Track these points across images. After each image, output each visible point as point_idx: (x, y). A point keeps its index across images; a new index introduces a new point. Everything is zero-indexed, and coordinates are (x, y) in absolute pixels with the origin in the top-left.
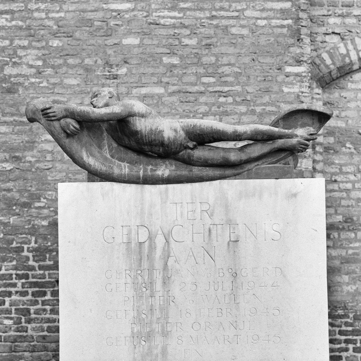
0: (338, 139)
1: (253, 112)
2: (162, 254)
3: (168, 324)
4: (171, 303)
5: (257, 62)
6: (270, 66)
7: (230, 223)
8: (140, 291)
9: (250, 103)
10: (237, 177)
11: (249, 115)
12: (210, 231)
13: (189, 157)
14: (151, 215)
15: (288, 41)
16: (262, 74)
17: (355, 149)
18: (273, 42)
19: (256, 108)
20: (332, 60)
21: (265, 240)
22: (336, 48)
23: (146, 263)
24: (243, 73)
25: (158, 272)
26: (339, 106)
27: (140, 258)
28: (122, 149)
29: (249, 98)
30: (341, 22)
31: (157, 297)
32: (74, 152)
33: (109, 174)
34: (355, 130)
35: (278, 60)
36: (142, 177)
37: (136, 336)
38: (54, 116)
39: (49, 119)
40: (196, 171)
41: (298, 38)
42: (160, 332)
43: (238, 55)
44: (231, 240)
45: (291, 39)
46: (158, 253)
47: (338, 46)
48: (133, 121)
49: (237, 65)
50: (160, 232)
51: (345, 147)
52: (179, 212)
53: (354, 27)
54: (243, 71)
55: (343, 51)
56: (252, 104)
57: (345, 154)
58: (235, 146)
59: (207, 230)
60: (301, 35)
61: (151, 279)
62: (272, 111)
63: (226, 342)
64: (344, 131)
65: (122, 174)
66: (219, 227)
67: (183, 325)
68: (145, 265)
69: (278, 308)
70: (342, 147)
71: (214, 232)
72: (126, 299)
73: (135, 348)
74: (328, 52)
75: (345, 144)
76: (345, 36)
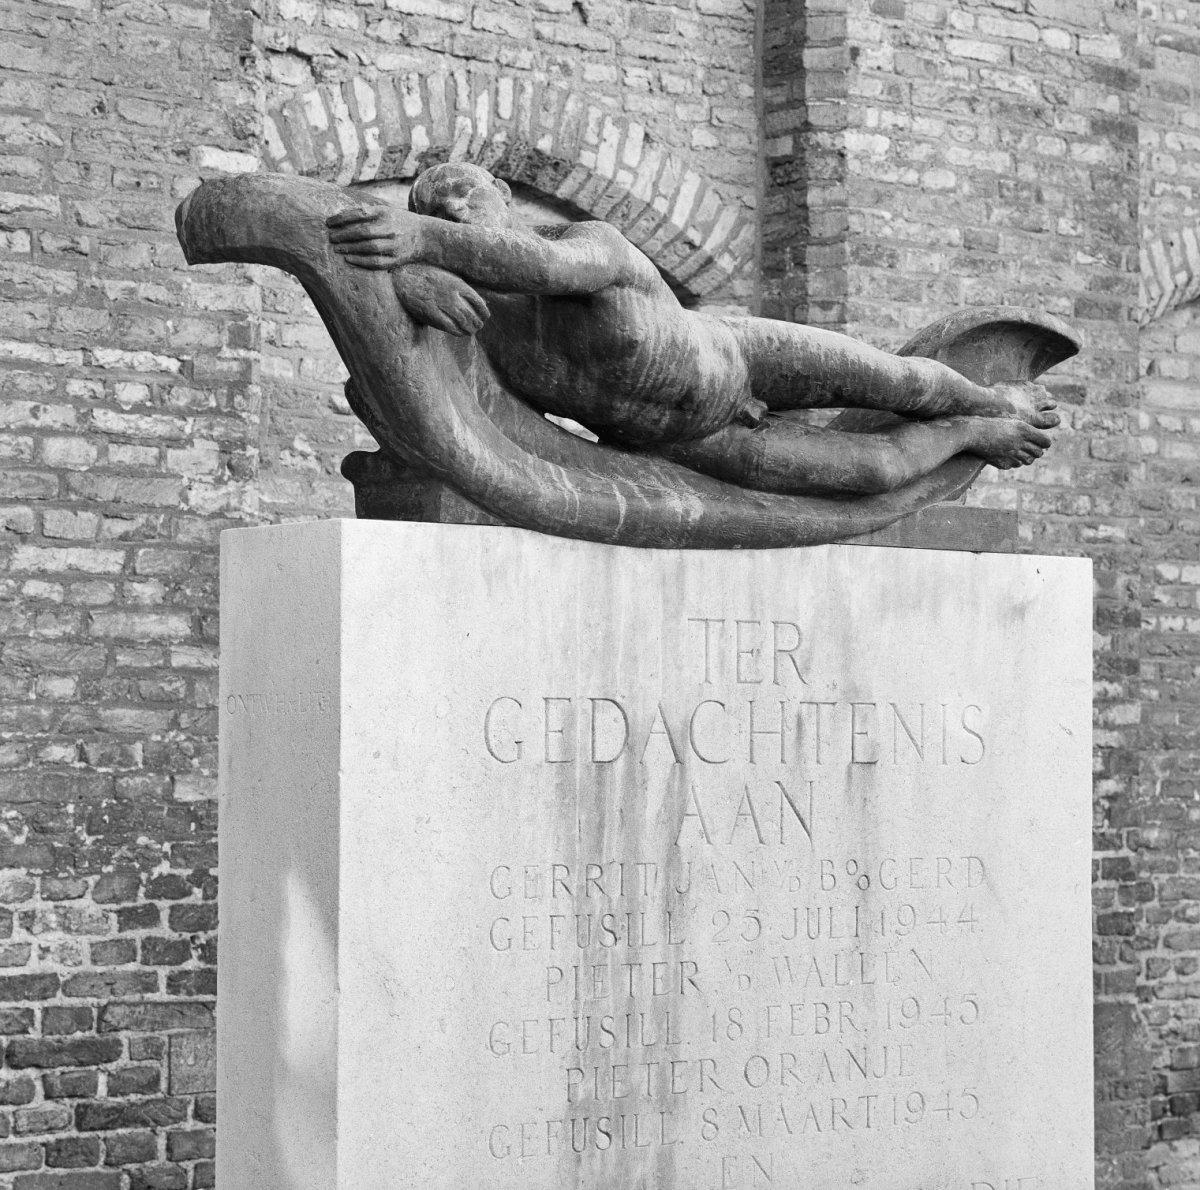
0: (272, 418)
1: (96, 297)
2: (665, 806)
3: (677, 1066)
4: (688, 987)
5: (113, 116)
6: (154, 138)
7: (855, 700)
8: (598, 946)
9: (87, 264)
10: (877, 537)
11: (83, 305)
12: (800, 724)
13: (745, 458)
14: (635, 659)
15: (213, 57)
16: (129, 164)
17: (318, 459)
18: (168, 53)
19: (107, 283)
20: (288, 147)
21: (944, 762)
22: (296, 103)
23: (616, 838)
24: (69, 151)
25: (651, 875)
26: (278, 308)
27: (598, 820)
28: (515, 403)
29: (85, 246)
30: (316, 16)
31: (647, 969)
32: (429, 402)
33: (525, 496)
34: (320, 394)
35: (180, 120)
36: (627, 517)
37: (580, 1116)
38: (389, 253)
39: (365, 260)
40: (745, 507)
41: (245, 53)
42: (654, 1097)
43: (54, 80)
44: (858, 759)
45: (221, 53)
46: (653, 803)
47: (306, 97)
48: (624, 304)
49: (48, 117)
50: (659, 726)
51: (292, 448)
52: (714, 652)
53: (355, 43)
54: (68, 142)
55: (318, 118)
56: (94, 267)
57: (290, 473)
58: (35, 416)
59: (792, 724)
60: (252, 42)
61: (630, 901)
62: (157, 301)
63: (840, 1124)
64: (291, 393)
65: (564, 500)
66: (825, 709)
67: (719, 1069)
68: (614, 845)
69: (973, 998)
70: (282, 449)
71: (810, 729)
72: (555, 975)
73: (579, 1160)
74: (277, 114)
75: (293, 440)
76: (326, 67)
